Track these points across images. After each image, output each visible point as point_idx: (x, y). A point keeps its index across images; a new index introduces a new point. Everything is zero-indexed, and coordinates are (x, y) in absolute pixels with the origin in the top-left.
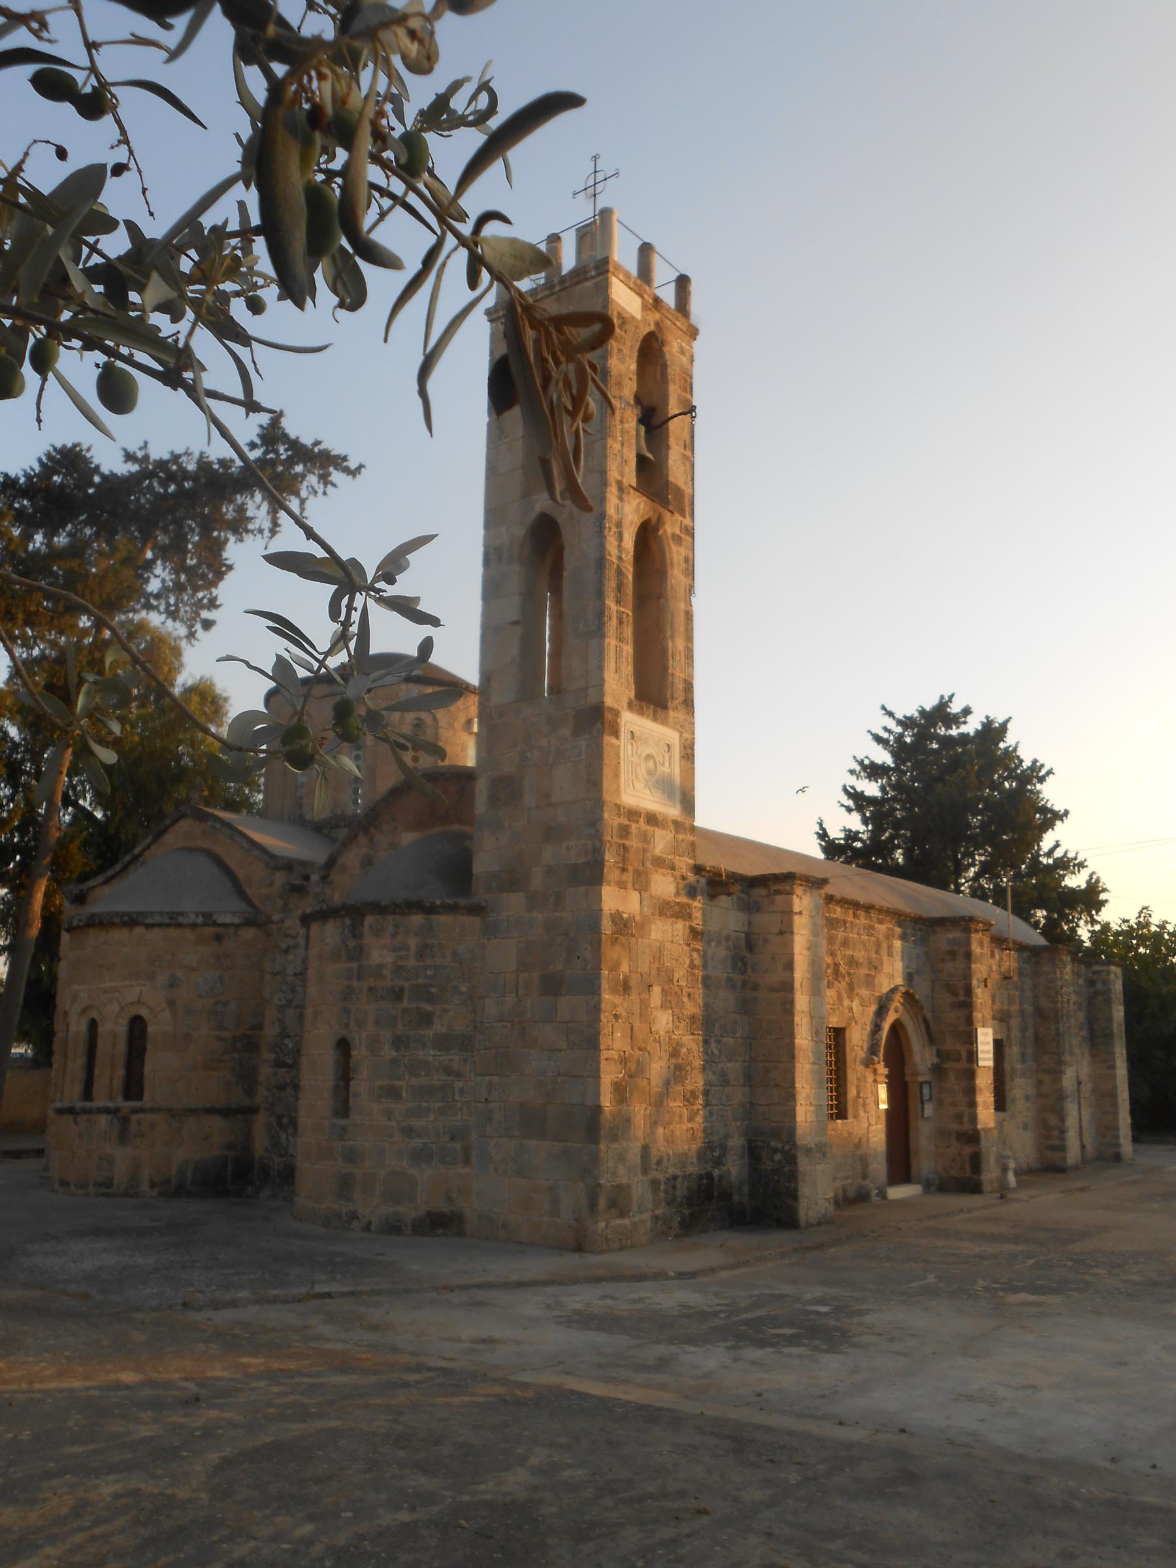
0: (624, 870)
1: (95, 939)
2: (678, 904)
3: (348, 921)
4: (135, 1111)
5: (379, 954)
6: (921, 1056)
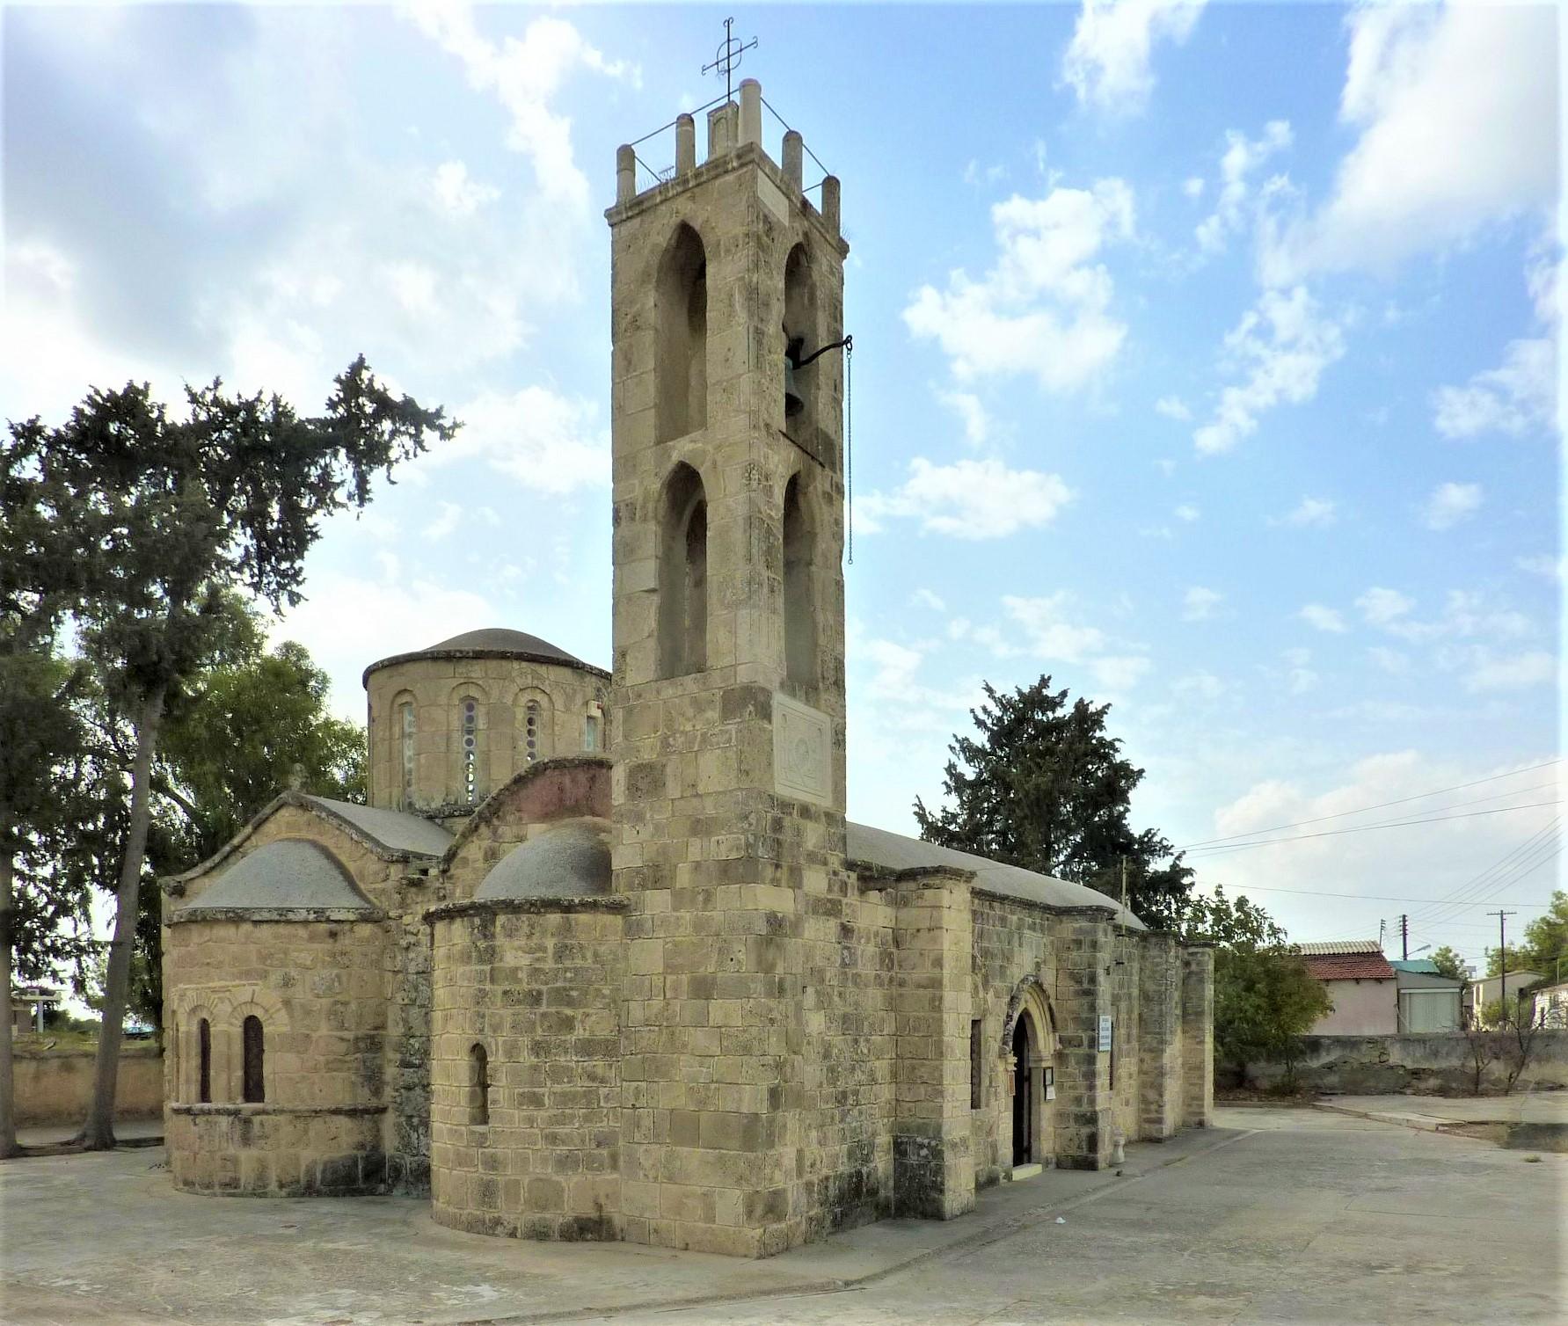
0: (777, 866)
1: (197, 935)
2: (829, 901)
3: (477, 921)
4: (258, 1113)
5: (513, 955)
6: (1045, 1043)
